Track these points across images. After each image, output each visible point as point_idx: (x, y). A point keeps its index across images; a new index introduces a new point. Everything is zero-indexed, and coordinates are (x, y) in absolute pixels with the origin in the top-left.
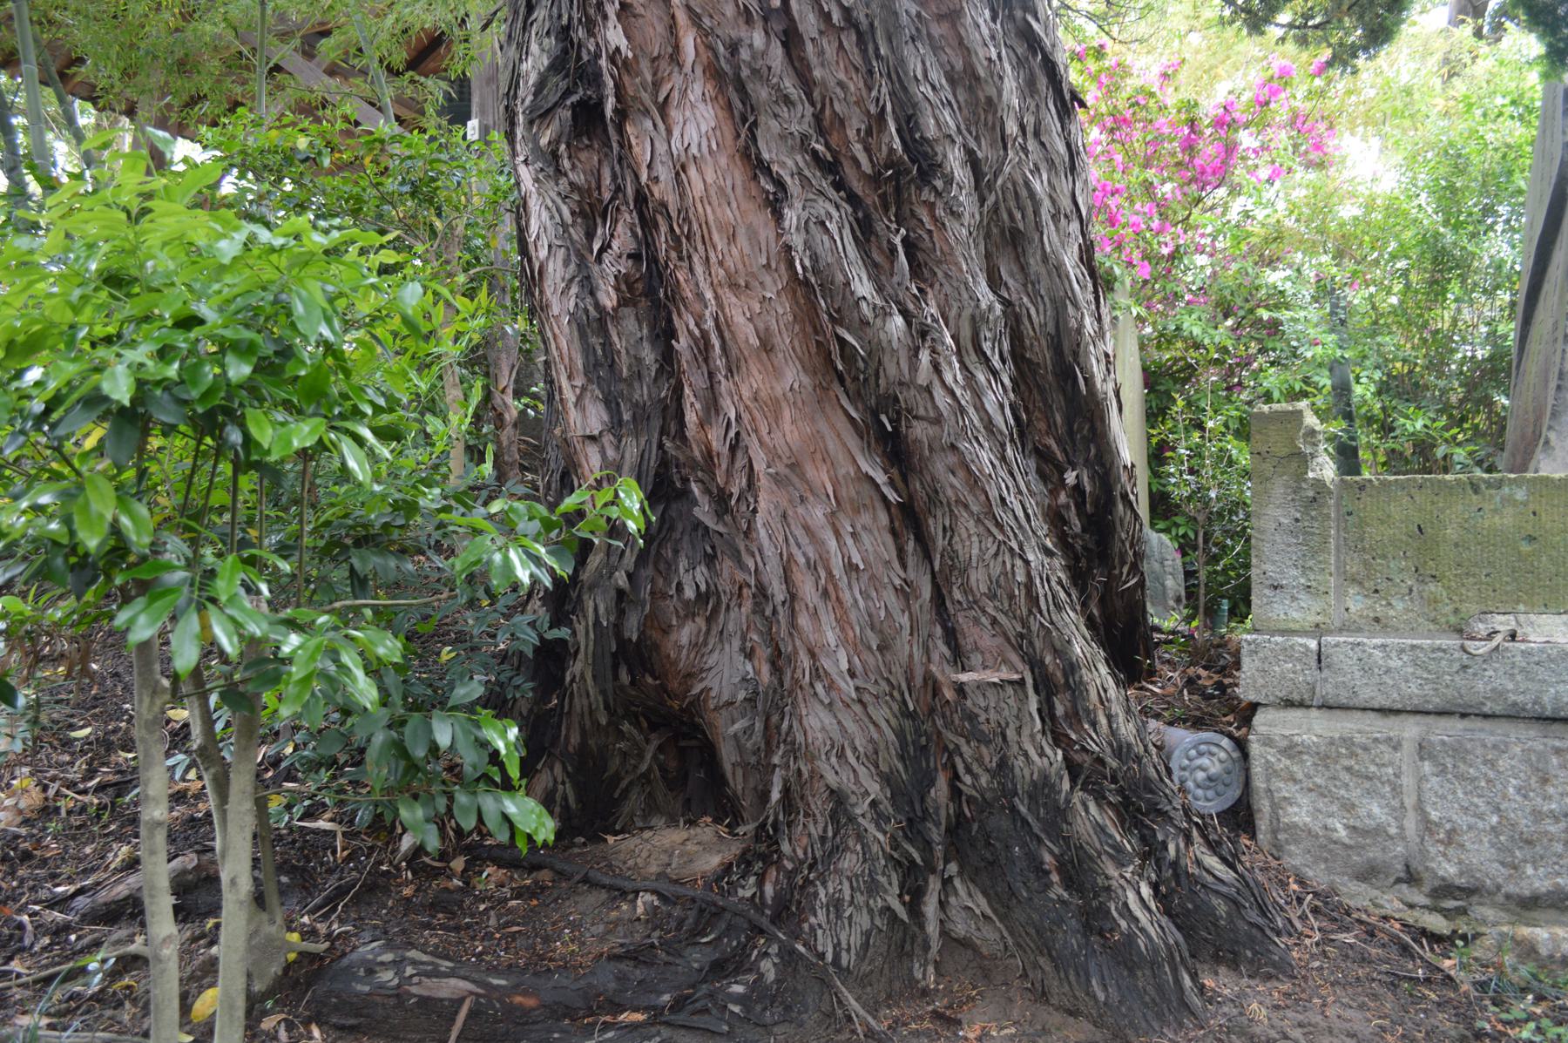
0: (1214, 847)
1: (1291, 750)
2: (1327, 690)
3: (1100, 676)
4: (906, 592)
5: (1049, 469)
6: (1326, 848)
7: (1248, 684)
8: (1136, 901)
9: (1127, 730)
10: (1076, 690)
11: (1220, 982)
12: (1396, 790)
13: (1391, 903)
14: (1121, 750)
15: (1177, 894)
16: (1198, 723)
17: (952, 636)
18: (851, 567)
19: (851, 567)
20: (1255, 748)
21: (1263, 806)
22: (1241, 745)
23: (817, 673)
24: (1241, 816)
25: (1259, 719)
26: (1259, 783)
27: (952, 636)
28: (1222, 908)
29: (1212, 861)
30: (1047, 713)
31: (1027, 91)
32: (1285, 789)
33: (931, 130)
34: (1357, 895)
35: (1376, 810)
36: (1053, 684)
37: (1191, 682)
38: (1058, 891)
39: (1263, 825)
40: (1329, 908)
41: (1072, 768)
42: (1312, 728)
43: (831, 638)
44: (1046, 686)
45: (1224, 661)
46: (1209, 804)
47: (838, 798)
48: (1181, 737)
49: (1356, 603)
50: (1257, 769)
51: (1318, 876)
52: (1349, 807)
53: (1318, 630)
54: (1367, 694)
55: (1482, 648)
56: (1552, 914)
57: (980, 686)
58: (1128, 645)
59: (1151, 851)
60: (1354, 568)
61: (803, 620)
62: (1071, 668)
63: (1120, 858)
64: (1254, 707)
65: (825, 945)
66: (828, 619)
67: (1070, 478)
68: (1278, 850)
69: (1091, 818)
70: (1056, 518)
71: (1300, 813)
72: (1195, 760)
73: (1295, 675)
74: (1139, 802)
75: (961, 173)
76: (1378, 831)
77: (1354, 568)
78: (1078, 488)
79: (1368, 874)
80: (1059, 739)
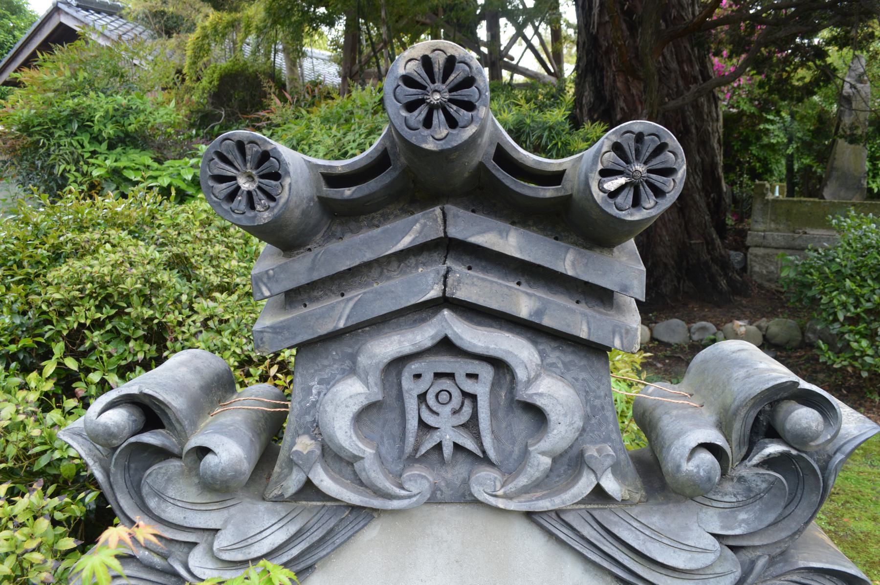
0: (738, 274)
1: (756, 256)
2: (765, 244)
3: (718, 241)
4: (680, 226)
5: (707, 194)
6: (761, 275)
7: (749, 241)
8: (723, 283)
9: (723, 252)
10: (713, 244)
11: (738, 298)
12: (777, 264)
13: (773, 286)
14: (722, 256)
15: (731, 282)
16: (736, 250)
17: (688, 233)
18: (669, 220)
19: (669, 220)
20: (749, 256)
21: (749, 267)
22: (745, 255)
23: (661, 240)
24: (744, 269)
25: (750, 250)
26: (749, 262)
27: (688, 233)
28: (739, 285)
29: (738, 277)
30: (708, 249)
31: (853, 554)
32: (754, 264)
33: (689, 123)
34: (767, 285)
35: (772, 268)
36: (709, 243)
37: (735, 240)
38: (708, 282)
39: (749, 271)
40: (760, 287)
41: (712, 259)
42: (760, 251)
43: (664, 233)
44: (708, 244)
45: (743, 234)
46: (738, 267)
47: (665, 265)
48: (732, 253)
49: (773, 226)
50: (748, 260)
51: (759, 281)
52: (767, 267)
53: (764, 231)
54: (773, 244)
55: (797, 236)
56: (342, 455)
57: (695, 244)
58: (721, 229)
59: (726, 275)
60: (773, 218)
61: (658, 230)
62: (713, 240)
63: (720, 276)
64: (749, 247)
65: (664, 290)
66: (664, 230)
67: (712, 195)
68: (751, 276)
69: (715, 268)
70: (708, 205)
71: (757, 268)
72: (736, 257)
73: (757, 240)
74: (725, 264)
75: (694, 131)
76: (773, 272)
77: (773, 218)
78: (713, 199)
79: (770, 280)
80: (709, 254)
